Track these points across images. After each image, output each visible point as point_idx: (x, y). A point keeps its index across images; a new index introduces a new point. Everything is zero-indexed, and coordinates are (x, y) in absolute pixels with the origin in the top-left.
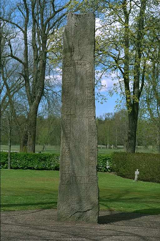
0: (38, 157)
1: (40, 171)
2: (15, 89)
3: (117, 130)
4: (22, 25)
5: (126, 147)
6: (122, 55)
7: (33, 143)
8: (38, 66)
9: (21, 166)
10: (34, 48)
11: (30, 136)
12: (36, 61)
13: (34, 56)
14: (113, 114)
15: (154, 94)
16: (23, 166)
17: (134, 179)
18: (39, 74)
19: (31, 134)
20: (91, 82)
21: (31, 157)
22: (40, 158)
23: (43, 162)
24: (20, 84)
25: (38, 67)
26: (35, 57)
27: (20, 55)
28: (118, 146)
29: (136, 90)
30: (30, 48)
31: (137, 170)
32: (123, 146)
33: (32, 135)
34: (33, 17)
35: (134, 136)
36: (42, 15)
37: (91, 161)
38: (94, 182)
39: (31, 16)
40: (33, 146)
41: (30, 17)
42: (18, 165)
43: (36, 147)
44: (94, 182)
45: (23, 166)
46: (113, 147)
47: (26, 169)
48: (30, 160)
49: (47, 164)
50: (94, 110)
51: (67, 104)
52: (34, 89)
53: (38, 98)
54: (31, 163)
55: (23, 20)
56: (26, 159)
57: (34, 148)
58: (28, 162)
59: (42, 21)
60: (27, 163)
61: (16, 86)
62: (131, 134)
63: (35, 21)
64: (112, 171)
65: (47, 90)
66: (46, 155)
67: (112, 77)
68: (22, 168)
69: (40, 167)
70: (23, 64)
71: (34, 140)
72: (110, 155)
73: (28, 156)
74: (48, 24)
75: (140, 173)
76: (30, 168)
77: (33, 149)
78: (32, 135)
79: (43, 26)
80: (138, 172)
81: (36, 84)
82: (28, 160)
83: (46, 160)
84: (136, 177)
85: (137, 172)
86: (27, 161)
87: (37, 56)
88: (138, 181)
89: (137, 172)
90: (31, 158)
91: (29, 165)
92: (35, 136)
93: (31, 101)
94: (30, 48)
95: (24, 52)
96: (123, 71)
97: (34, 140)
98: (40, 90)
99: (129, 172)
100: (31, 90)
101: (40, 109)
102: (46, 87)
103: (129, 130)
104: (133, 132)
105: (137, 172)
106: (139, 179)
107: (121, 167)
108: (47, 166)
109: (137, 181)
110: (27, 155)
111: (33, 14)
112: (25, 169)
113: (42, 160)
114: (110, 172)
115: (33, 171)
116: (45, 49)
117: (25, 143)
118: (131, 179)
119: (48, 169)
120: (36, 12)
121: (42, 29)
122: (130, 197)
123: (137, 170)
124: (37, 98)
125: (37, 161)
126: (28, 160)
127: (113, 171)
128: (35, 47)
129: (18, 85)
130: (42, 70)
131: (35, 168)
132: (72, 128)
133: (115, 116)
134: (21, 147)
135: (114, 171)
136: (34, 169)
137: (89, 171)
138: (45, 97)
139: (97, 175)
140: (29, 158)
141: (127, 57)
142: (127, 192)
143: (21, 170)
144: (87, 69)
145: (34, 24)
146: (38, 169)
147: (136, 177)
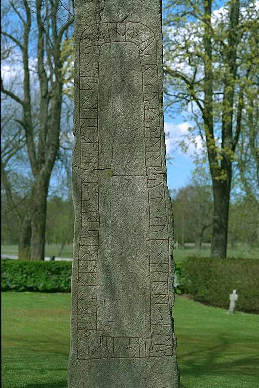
0: (44, 268)
1: (49, 294)
2: (10, 150)
3: (183, 217)
4: (19, 35)
5: (199, 245)
6: (200, 76)
7: (41, 242)
8: (49, 108)
9: (14, 286)
10: (40, 76)
11: (36, 228)
12: (45, 100)
13: (41, 90)
14: (177, 192)
15: (252, 154)
16: (17, 285)
17: (227, 307)
18: (50, 123)
19: (37, 226)
20: (153, 80)
21: (32, 267)
22: (49, 270)
23: (54, 277)
24: (20, 141)
25: (48, 110)
26: (44, 93)
27: (19, 92)
28: (186, 244)
29: (227, 141)
30: (34, 76)
31: (234, 291)
32: (193, 244)
33: (39, 227)
34: (40, 24)
35: (225, 227)
36: (54, 22)
37: (155, 296)
38: (165, 353)
39: (36, 22)
40: (41, 247)
41: (34, 26)
42: (7, 283)
43: (46, 246)
44: (165, 353)
45: (17, 285)
46: (178, 246)
47: (23, 291)
48: (31, 274)
49: (62, 281)
50: (163, 156)
51: (88, 141)
52: (42, 148)
53: (48, 162)
54: (33, 279)
55: (20, 28)
56: (22, 271)
57: (43, 251)
58: (26, 278)
59: (55, 31)
60: (24, 280)
61: (13, 145)
62: (220, 222)
63: (42, 30)
64: (183, 291)
65: (65, 148)
66: (60, 264)
67: (183, 117)
68: (16, 289)
69: (49, 286)
70: (22, 103)
71: (43, 236)
72: (180, 262)
73: (26, 267)
74: (64, 35)
75: (239, 297)
76: (31, 289)
77: (41, 252)
78: (39, 227)
79: (55, 37)
80: (236, 296)
81: (45, 139)
82: (27, 274)
83: (60, 274)
84: (232, 305)
85: (234, 296)
86: (25, 275)
87: (46, 91)
88: (236, 312)
89: (234, 296)
90: (33, 269)
91: (29, 282)
92: (43, 229)
93: (37, 164)
94: (34, 76)
95: (198, 377)
96: (203, 107)
97: (43, 236)
98: (52, 149)
99: (216, 294)
100: (37, 150)
101: (53, 182)
102: (62, 143)
103: (215, 215)
104: (223, 220)
105: (233, 295)
106: (237, 308)
107: (200, 284)
108: (62, 285)
109: (234, 312)
110: (25, 265)
111: (39, 16)
112: (21, 291)
113: (53, 273)
114: (180, 294)
115: (36, 295)
116: (60, 77)
117: (27, 241)
118: (220, 307)
119: (64, 290)
120: (43, 15)
121: (55, 42)
122: (237, 358)
123: (234, 291)
124: (46, 163)
125: (43, 276)
126: (27, 274)
127: (186, 292)
128: (43, 75)
129: (16, 143)
130: (55, 114)
131: (40, 288)
132: (102, 207)
133: (179, 194)
134: (21, 248)
135: (188, 293)
136: (38, 290)
137: (150, 322)
138: (62, 161)
139: (173, 331)
140: (28, 270)
141: (209, 76)
142: (225, 342)
143: (13, 292)
144: (143, 46)
145: (41, 36)
146: (45, 291)
147: (232, 305)
